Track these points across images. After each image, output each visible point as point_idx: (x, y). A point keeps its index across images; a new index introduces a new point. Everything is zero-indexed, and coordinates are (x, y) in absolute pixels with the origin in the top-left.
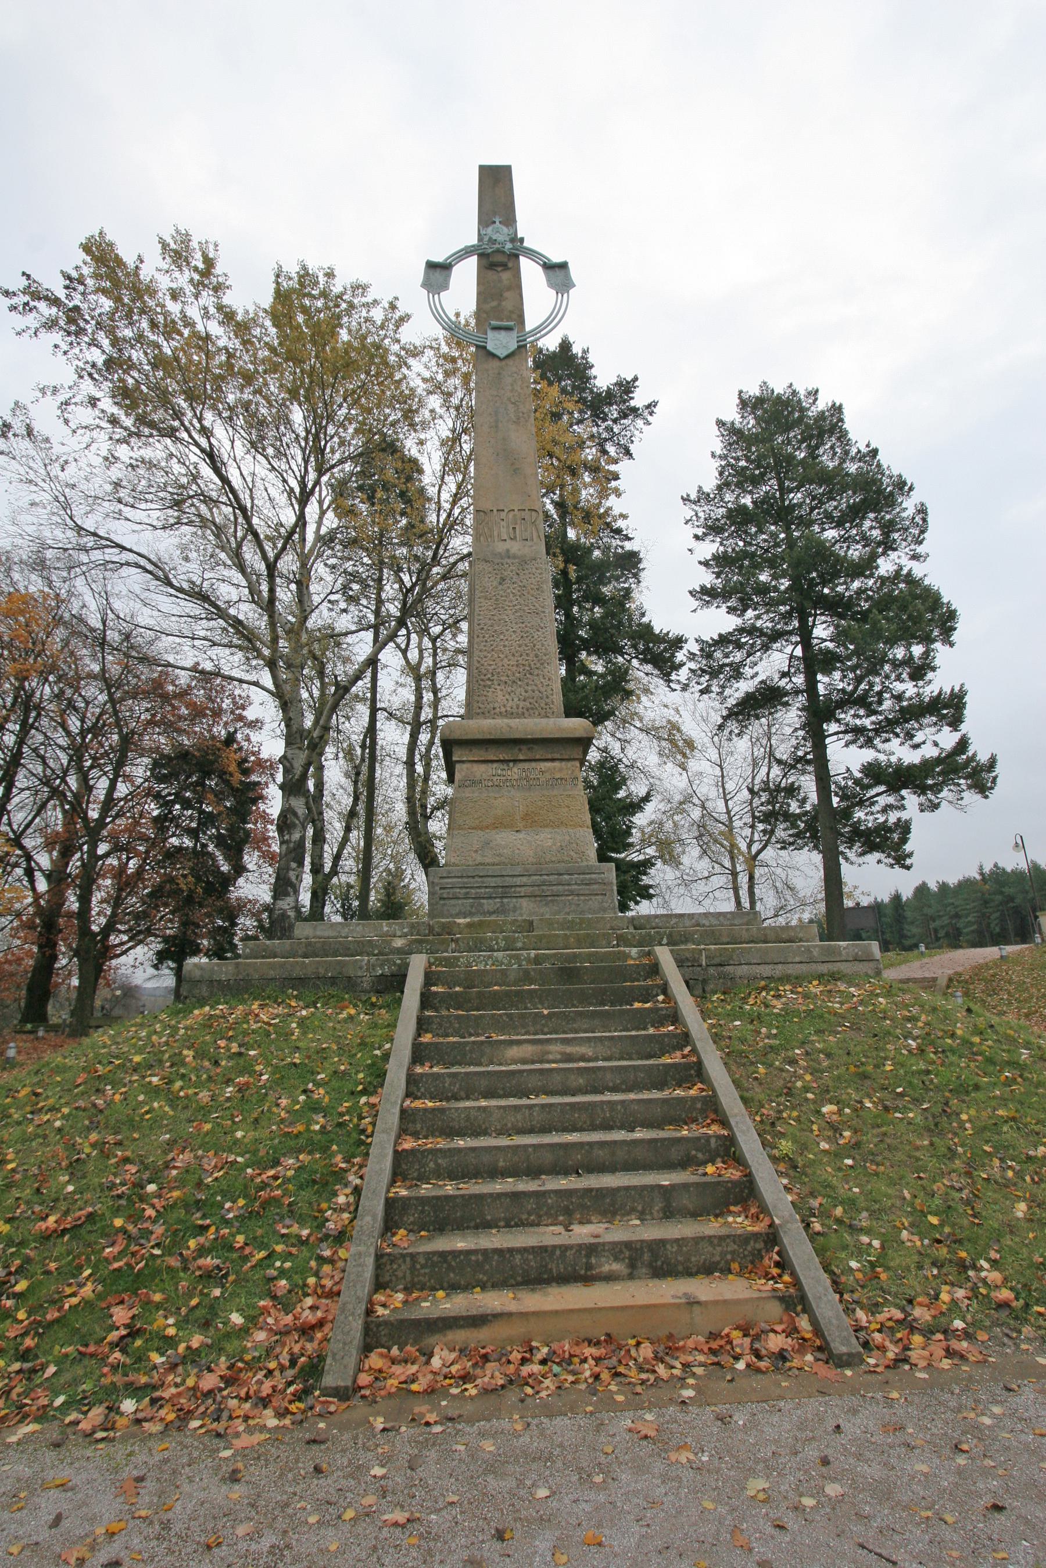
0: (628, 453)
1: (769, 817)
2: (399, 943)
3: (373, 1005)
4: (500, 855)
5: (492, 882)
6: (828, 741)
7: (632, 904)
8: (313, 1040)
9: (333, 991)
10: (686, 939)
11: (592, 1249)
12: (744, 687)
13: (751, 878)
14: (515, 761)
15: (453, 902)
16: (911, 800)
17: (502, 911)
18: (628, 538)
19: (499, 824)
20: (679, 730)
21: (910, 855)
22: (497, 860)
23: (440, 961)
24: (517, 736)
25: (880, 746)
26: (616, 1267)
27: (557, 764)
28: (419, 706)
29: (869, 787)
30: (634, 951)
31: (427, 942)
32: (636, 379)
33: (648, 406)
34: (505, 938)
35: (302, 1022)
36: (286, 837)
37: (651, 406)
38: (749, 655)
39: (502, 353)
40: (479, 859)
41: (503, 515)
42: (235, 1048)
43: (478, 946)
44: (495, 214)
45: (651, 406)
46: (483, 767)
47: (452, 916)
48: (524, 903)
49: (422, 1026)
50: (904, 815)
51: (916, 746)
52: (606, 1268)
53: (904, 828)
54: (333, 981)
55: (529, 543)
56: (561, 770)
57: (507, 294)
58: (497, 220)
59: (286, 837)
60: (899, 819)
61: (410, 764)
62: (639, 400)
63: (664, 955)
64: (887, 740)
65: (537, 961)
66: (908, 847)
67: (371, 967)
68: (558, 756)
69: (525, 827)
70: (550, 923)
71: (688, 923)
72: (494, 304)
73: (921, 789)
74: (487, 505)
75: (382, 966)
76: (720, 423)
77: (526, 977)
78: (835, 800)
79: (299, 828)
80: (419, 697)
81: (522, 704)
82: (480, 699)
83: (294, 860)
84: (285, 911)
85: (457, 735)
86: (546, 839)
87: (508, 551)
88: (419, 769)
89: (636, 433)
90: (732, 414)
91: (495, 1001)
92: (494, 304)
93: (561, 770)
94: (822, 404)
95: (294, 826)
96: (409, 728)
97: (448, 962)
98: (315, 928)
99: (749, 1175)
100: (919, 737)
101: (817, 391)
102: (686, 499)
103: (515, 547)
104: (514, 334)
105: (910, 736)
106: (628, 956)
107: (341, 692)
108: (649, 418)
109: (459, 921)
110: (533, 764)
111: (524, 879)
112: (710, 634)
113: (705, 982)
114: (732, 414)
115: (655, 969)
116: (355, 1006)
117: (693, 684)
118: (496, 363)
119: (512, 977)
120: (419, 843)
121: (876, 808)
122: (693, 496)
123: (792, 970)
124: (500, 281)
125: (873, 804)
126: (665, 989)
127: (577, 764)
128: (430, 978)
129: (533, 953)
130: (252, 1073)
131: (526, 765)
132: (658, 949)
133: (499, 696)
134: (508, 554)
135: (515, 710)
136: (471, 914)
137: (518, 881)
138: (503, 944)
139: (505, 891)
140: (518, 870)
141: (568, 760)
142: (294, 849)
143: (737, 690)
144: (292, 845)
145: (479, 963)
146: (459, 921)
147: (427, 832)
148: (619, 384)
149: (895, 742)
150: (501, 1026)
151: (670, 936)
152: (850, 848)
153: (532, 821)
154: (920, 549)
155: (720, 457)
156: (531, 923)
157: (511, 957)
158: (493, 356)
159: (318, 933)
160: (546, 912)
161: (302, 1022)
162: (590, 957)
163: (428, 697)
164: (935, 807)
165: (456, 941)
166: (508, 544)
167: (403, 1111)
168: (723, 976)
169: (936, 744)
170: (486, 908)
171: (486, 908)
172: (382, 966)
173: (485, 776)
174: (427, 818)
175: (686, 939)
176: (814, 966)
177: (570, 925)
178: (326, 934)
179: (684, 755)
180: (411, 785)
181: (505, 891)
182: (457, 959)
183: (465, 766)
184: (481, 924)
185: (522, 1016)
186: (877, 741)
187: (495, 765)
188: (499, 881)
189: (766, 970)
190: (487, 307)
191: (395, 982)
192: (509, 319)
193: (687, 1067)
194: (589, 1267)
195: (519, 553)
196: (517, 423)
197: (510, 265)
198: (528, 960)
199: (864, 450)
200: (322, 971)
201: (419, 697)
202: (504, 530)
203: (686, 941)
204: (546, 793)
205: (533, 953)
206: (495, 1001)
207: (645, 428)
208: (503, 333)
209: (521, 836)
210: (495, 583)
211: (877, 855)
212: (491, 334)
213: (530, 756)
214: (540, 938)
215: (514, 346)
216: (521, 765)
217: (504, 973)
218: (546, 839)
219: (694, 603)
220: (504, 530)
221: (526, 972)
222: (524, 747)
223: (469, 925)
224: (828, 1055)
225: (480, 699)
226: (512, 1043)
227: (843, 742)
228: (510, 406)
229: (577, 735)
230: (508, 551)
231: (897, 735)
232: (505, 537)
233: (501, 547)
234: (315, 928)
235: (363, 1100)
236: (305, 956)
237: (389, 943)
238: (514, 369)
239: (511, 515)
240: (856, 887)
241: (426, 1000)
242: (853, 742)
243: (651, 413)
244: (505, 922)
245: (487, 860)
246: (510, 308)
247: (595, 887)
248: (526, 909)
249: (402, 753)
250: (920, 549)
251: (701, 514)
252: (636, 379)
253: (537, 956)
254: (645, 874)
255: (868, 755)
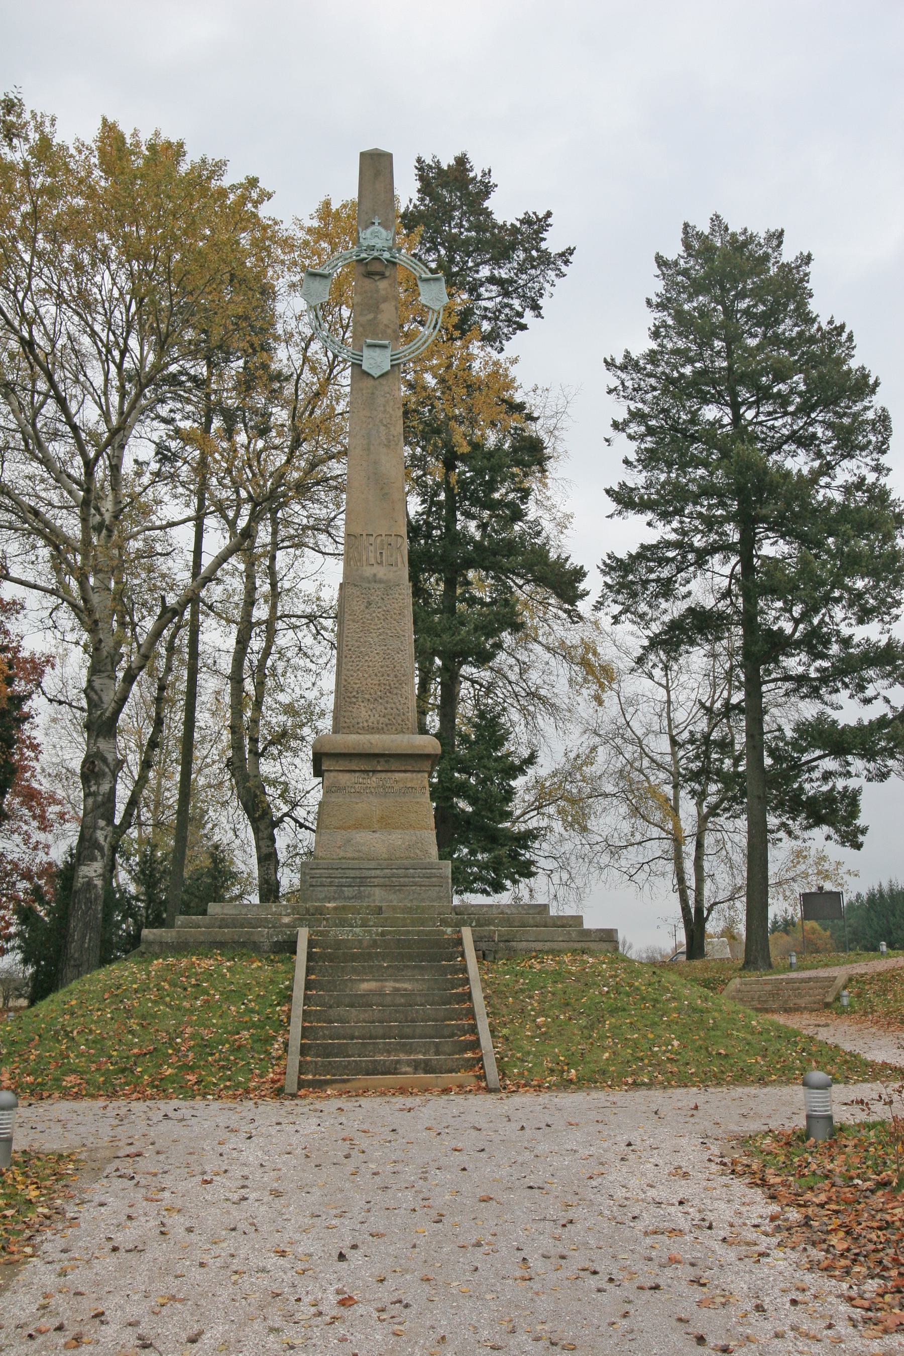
0: (536, 307)
1: (703, 775)
2: (286, 920)
3: (272, 961)
4: (359, 851)
5: (352, 873)
6: (764, 688)
7: (508, 883)
8: (240, 979)
9: (244, 951)
10: (489, 922)
11: (398, 1062)
12: (674, 609)
13: (700, 846)
14: (374, 771)
15: (319, 889)
16: (858, 764)
17: (359, 897)
18: (531, 418)
19: (359, 826)
20: (595, 653)
21: (863, 831)
22: (356, 855)
23: (318, 933)
24: (377, 751)
25: (827, 697)
26: (408, 1069)
27: (408, 775)
28: (250, 602)
29: (803, 751)
30: (449, 930)
31: (306, 919)
32: (549, 214)
33: (562, 255)
34: (361, 919)
35: (229, 969)
36: (93, 788)
37: (566, 255)
38: (680, 571)
39: (376, 373)
40: (342, 854)
41: (372, 539)
42: (193, 981)
43: (343, 923)
44: (375, 212)
45: (566, 255)
46: (347, 776)
47: (318, 900)
48: (377, 890)
49: (309, 971)
50: (853, 783)
51: (867, 701)
52: (403, 1070)
53: (852, 799)
54: (244, 944)
55: (394, 569)
56: (412, 780)
57: (383, 306)
58: (377, 221)
59: (93, 788)
60: (845, 788)
61: (236, 679)
62: (553, 243)
63: (467, 933)
64: (837, 691)
65: (383, 934)
66: (860, 822)
67: (269, 936)
68: (410, 768)
69: (381, 828)
70: (394, 908)
71: (495, 911)
72: (371, 316)
73: (869, 754)
74: (358, 530)
75: (277, 936)
76: (661, 262)
77: (375, 944)
78: (768, 761)
79: (109, 777)
80: (251, 589)
81: (382, 720)
82: (346, 714)
83: (103, 817)
84: (91, 879)
85: (326, 749)
86: (397, 839)
87: (375, 575)
88: (249, 686)
89: (546, 285)
90: (674, 250)
91: (354, 958)
92: (371, 316)
93: (412, 780)
94: (788, 254)
95: (104, 775)
96: (234, 628)
97: (321, 933)
98: (223, 907)
99: (478, 1039)
100: (870, 692)
101: (782, 233)
102: (610, 364)
103: (381, 572)
104: (388, 353)
105: (861, 688)
106: (444, 933)
107: (169, 615)
108: (564, 268)
109: (328, 905)
110: (389, 774)
111: (378, 872)
112: (625, 548)
113: (496, 952)
114: (674, 250)
115: (460, 942)
116: (260, 961)
117: (609, 602)
118: (370, 383)
119: (365, 944)
120: (248, 790)
121: (816, 774)
122: (619, 361)
123: (555, 946)
124: (377, 291)
125: (813, 769)
126: (463, 955)
127: (426, 775)
128: (311, 944)
129: (380, 929)
130: (208, 994)
131: (383, 775)
132: (464, 929)
133: (363, 713)
134: (375, 579)
135: (375, 725)
136: (335, 899)
137: (373, 873)
138: (359, 922)
139: (362, 881)
140: (373, 864)
141: (419, 772)
142: (103, 804)
143: (665, 611)
144: (100, 798)
145: (343, 934)
146: (328, 905)
147: (257, 775)
148: (527, 221)
149: (845, 693)
150: (355, 971)
151: (478, 920)
152: (794, 820)
153: (386, 823)
154: (884, 460)
155: (658, 305)
156: (380, 908)
157: (365, 931)
158: (368, 375)
159: (225, 911)
160: (394, 899)
161: (229, 969)
162: (418, 933)
163: (263, 587)
164: (883, 776)
165: (327, 919)
166: (376, 569)
167: (304, 1011)
168: (509, 949)
169: (887, 701)
170: (346, 894)
171: (346, 894)
172: (277, 936)
173: (348, 784)
174: (257, 755)
175: (489, 922)
176: (572, 944)
177: (410, 910)
178: (231, 912)
179: (601, 685)
180: (237, 707)
181: (362, 881)
182: (328, 932)
183: (332, 774)
184: (344, 907)
185: (372, 967)
186: (823, 691)
187: (357, 774)
188: (357, 873)
189: (539, 946)
190: (363, 319)
191: (291, 947)
192: (384, 336)
193: (463, 994)
194: (396, 1069)
195: (385, 578)
196: (388, 446)
197: (387, 274)
198: (377, 934)
199: (825, 327)
200: (236, 937)
201: (251, 589)
202: (371, 555)
203: (488, 925)
204: (398, 799)
205: (380, 929)
206: (354, 958)
207: (557, 281)
208: (378, 350)
209: (377, 835)
210: (362, 607)
211: (826, 829)
212: (366, 352)
213: (387, 767)
214: (386, 919)
215: (387, 367)
216: (379, 775)
217: (360, 941)
218: (397, 839)
219: (613, 506)
220: (371, 555)
221: (375, 941)
222: (382, 760)
223: (335, 908)
224: (553, 994)
225: (346, 714)
226: (364, 980)
227: (782, 692)
228: (382, 428)
229: (427, 751)
230: (375, 575)
231: (846, 686)
232: (372, 561)
233: (368, 571)
234: (223, 907)
235: (278, 1008)
236: (220, 927)
237: (279, 920)
238: (387, 389)
239: (379, 539)
240: (838, 863)
241: (310, 957)
242: (795, 690)
243: (566, 262)
244: (361, 907)
245: (349, 855)
246: (386, 322)
247: (434, 879)
248: (378, 896)
249: (226, 664)
250: (884, 460)
251: (629, 384)
252: (549, 214)
253: (383, 931)
254: (526, 847)
255: (809, 710)
